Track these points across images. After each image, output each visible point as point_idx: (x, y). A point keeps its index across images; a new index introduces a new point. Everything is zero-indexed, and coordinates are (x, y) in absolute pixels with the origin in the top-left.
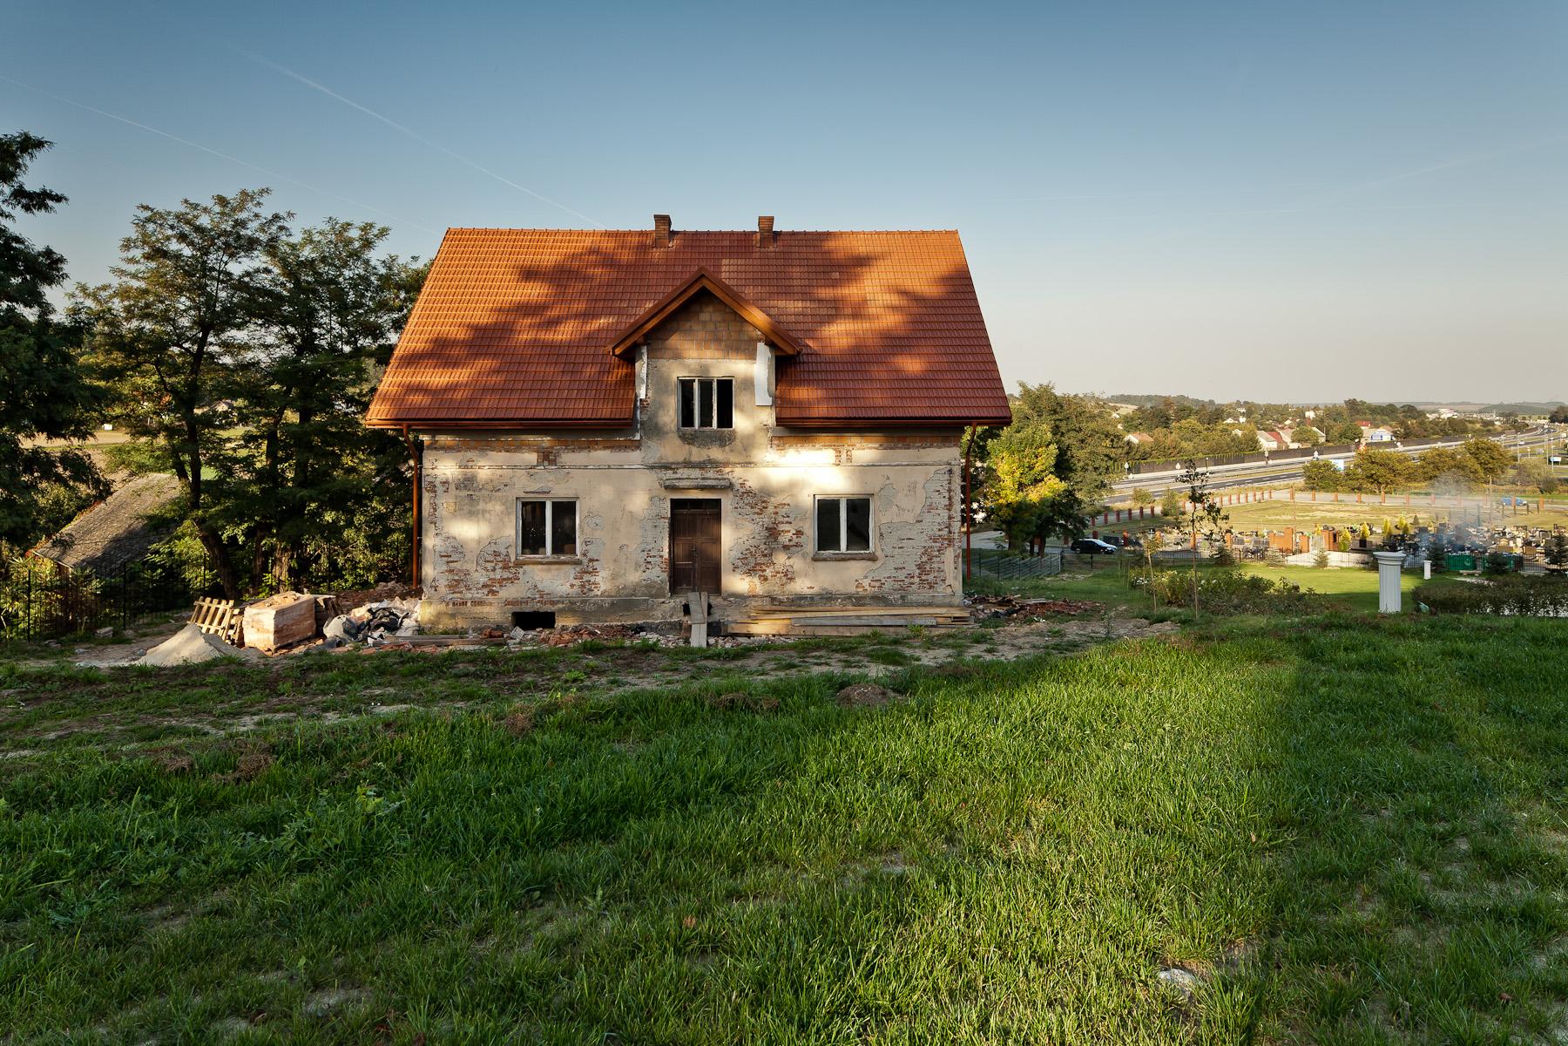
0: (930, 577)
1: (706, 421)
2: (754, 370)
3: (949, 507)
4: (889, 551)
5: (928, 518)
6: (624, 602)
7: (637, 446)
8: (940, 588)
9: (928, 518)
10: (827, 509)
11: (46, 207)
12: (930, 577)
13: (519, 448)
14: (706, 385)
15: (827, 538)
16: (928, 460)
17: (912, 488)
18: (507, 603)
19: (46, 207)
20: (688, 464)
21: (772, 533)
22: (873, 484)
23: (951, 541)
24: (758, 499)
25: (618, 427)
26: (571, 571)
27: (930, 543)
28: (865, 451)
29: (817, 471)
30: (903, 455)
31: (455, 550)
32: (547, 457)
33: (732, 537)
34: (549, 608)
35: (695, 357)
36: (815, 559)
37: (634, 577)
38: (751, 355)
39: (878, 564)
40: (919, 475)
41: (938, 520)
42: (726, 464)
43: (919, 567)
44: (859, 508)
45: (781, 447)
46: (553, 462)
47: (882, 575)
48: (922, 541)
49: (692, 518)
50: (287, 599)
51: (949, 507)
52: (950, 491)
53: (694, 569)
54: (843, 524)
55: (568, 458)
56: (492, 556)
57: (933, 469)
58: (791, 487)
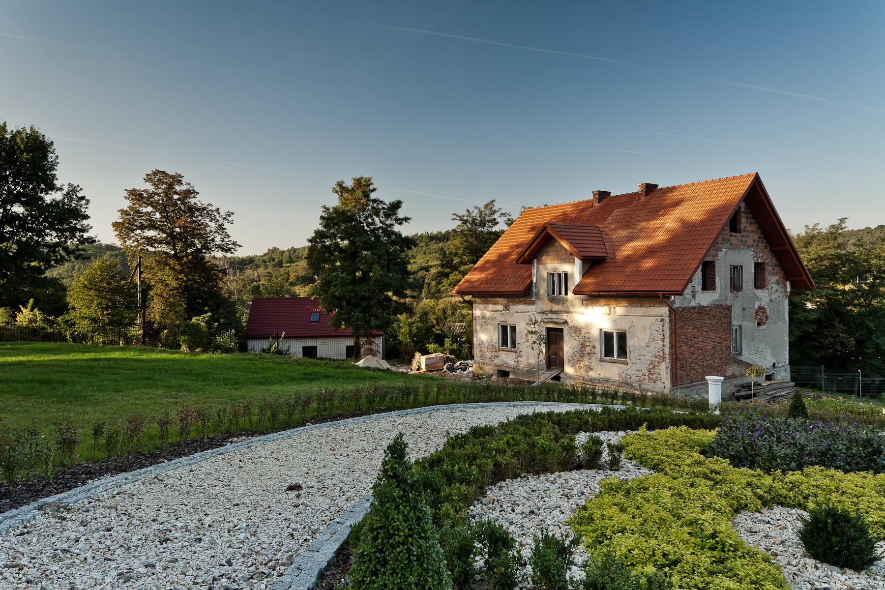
0: (654, 377)
1: (560, 293)
2: (574, 270)
3: (663, 339)
4: (633, 360)
5: (652, 345)
6: (530, 371)
7: (533, 303)
8: (659, 383)
9: (652, 345)
10: (608, 337)
11: (310, 241)
12: (654, 377)
13: (496, 303)
14: (560, 275)
15: (608, 351)
16: (652, 313)
17: (644, 328)
18: (496, 366)
19: (310, 241)
20: (552, 312)
21: (583, 346)
22: (624, 326)
23: (664, 358)
24: (577, 330)
25: (526, 294)
26: (514, 355)
27: (653, 359)
28: (620, 310)
29: (596, 318)
30: (639, 310)
31: (481, 344)
32: (506, 308)
33: (569, 347)
34: (507, 370)
35: (550, 265)
36: (601, 361)
37: (532, 361)
38: (572, 262)
39: (629, 366)
40: (648, 321)
41: (658, 346)
42: (561, 312)
43: (649, 370)
44: (622, 337)
45: (587, 305)
46: (508, 309)
47: (631, 372)
48: (649, 357)
49: (554, 337)
50: (623, 456)
51: (663, 339)
52: (663, 331)
53: (554, 361)
54: (615, 345)
55: (513, 308)
56: (492, 347)
57: (655, 318)
58: (587, 326)
